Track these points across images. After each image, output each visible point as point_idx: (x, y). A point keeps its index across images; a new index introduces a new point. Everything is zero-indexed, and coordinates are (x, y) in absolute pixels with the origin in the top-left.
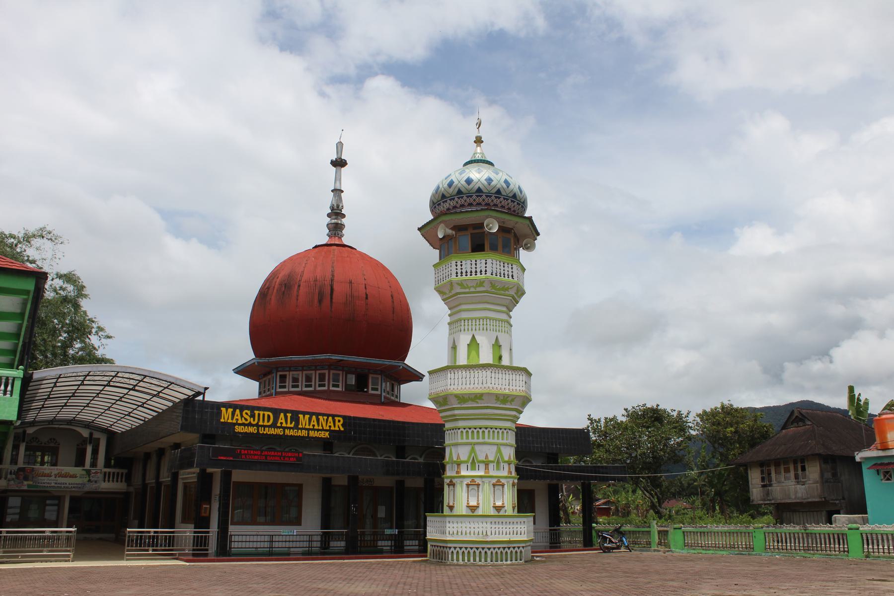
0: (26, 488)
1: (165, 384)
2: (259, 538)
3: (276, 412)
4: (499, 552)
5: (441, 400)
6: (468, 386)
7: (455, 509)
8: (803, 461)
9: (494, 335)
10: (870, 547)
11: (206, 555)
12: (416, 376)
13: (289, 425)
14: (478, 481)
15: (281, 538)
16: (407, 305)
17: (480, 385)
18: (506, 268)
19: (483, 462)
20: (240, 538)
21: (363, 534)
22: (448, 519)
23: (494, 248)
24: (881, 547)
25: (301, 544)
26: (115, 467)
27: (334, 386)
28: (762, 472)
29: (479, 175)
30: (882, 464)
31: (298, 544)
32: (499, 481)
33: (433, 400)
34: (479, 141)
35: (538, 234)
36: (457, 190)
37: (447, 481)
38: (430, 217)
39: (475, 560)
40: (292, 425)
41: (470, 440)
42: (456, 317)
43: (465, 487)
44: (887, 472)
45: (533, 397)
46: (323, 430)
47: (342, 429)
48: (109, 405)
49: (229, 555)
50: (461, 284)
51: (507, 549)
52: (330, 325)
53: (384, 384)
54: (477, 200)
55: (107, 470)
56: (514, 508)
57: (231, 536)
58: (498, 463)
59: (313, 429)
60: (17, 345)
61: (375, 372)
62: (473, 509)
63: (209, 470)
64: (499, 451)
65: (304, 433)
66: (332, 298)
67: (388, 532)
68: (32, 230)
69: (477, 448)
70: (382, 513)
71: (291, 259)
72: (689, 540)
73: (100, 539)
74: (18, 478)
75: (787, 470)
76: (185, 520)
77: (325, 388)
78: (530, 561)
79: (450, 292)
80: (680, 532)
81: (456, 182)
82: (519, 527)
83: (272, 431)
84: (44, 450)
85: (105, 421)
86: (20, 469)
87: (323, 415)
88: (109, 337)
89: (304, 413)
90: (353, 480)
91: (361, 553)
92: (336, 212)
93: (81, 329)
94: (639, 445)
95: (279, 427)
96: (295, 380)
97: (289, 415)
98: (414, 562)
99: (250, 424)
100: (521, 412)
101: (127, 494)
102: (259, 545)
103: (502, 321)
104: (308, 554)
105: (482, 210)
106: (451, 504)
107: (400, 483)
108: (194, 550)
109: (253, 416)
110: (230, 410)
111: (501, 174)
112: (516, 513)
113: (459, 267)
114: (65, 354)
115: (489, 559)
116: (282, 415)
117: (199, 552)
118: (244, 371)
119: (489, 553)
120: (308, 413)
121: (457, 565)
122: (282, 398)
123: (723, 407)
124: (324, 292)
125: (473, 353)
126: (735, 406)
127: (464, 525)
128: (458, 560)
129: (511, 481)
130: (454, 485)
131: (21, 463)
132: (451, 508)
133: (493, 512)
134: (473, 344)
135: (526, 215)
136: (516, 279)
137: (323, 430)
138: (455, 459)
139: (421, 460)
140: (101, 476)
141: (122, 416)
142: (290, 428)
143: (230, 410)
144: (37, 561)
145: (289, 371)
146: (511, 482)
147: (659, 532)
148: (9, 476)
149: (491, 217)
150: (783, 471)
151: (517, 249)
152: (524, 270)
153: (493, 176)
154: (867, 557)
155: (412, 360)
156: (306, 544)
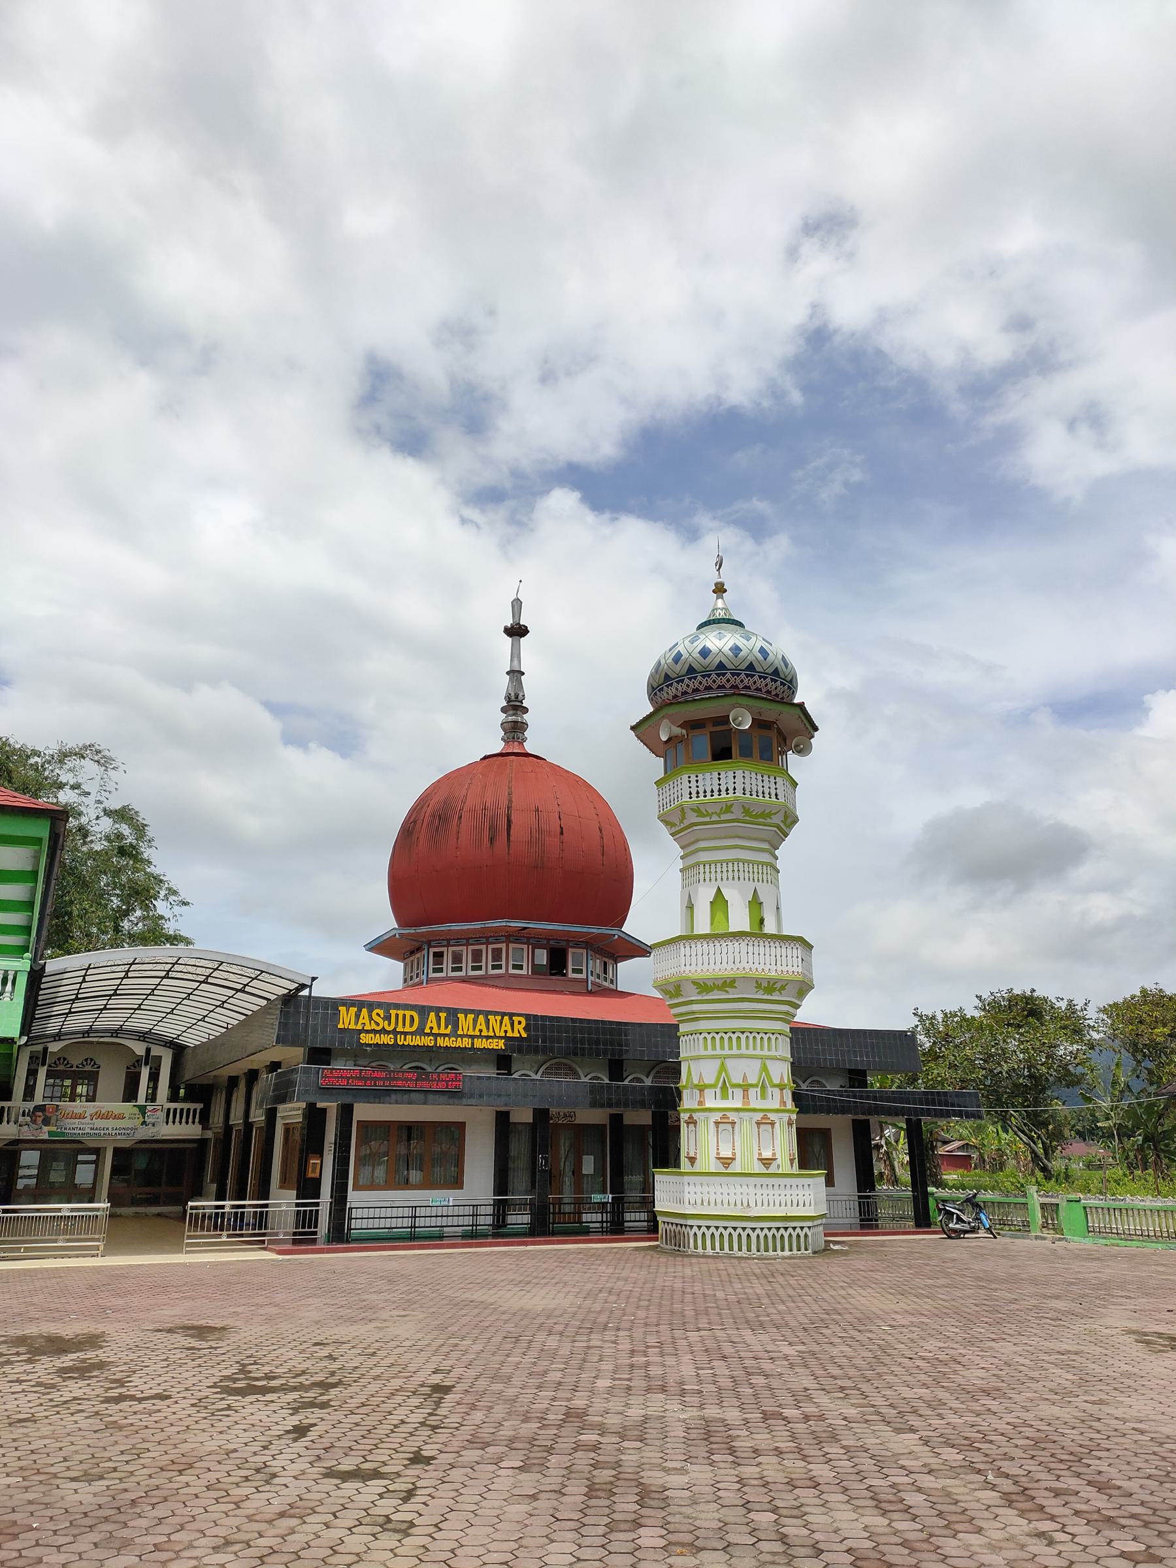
0: (46, 1137)
1: (253, 974)
2: (395, 1212)
3: (424, 1011)
4: (770, 1235)
5: (672, 988)
6: (706, 966)
7: (697, 1162)
9: (751, 886)
11: (314, 1241)
12: (638, 950)
13: (442, 1031)
14: (732, 1116)
15: (428, 1212)
16: (626, 849)
17: (731, 965)
18: (766, 784)
19: (739, 1086)
20: (365, 1213)
21: (560, 1202)
22: (686, 1179)
23: (746, 753)
25: (461, 1221)
26: (185, 1099)
27: (515, 967)
29: (720, 642)
31: (455, 1221)
33: (659, 988)
34: (720, 590)
35: (816, 729)
36: (687, 666)
37: (684, 1116)
38: (650, 709)
39: (731, 1249)
40: (448, 1031)
42: (691, 860)
43: (712, 1126)
45: (817, 975)
46: (495, 1037)
47: (524, 1035)
48: (173, 1006)
49: (348, 1242)
50: (697, 810)
51: (782, 1231)
52: (500, 871)
53: (591, 962)
54: (718, 682)
55: (173, 1105)
56: (792, 1161)
57: (351, 1209)
58: (763, 1087)
59: (480, 1036)
60: (31, 918)
61: (577, 945)
62: (727, 1162)
63: (320, 1105)
64: (764, 1068)
65: (466, 1043)
66: (509, 835)
67: (597, 1198)
68: (72, 743)
69: (729, 1063)
70: (588, 1165)
71: (448, 778)
72: (1095, 1221)
73: (159, 1215)
74: (34, 1122)
76: (284, 1184)
77: (502, 971)
78: (824, 1251)
79: (681, 822)
80: (1078, 1208)
81: (685, 655)
82: (801, 1193)
83: (418, 1041)
84: (77, 1076)
85: (169, 1029)
86: (41, 1108)
87: (496, 1013)
88: (185, 904)
89: (466, 1012)
90: (541, 1115)
91: (553, 1234)
92: (515, 704)
93: (142, 893)
94: (1004, 1055)
95: (428, 1035)
96: (457, 958)
97: (443, 1015)
98: (637, 1249)
99: (384, 1031)
100: (797, 1007)
101: (203, 1143)
102: (394, 1223)
103: (763, 864)
104: (472, 1236)
105: (726, 696)
107: (616, 1119)
108: (295, 1234)
109: (388, 1018)
110: (353, 1010)
111: (754, 639)
112: (795, 1170)
113: (693, 784)
114: (117, 929)
115: (754, 1247)
116: (432, 1015)
117: (304, 1234)
118: (381, 947)
119: (753, 1236)
120: (471, 1011)
121: (704, 1256)
122: (435, 988)
123: (1144, 992)
124: (499, 826)
125: (720, 916)
126: (1168, 992)
127: (712, 1189)
128: (704, 1248)
129: (785, 1117)
130: (695, 1123)
131: (38, 1100)
132: (692, 1160)
133: (758, 1168)
134: (719, 902)
135: (796, 701)
136: (782, 800)
137: (495, 1037)
138: (696, 1082)
139: (648, 1082)
140: (162, 1115)
141: (195, 1023)
142: (445, 1035)
143: (353, 1010)
144: (48, 1257)
145: (448, 946)
146: (786, 1119)
147: (1043, 1206)
148: (21, 1119)
149: (741, 706)
151: (784, 753)
152: (795, 784)
153: (741, 642)
155: (637, 925)
156: (468, 1220)
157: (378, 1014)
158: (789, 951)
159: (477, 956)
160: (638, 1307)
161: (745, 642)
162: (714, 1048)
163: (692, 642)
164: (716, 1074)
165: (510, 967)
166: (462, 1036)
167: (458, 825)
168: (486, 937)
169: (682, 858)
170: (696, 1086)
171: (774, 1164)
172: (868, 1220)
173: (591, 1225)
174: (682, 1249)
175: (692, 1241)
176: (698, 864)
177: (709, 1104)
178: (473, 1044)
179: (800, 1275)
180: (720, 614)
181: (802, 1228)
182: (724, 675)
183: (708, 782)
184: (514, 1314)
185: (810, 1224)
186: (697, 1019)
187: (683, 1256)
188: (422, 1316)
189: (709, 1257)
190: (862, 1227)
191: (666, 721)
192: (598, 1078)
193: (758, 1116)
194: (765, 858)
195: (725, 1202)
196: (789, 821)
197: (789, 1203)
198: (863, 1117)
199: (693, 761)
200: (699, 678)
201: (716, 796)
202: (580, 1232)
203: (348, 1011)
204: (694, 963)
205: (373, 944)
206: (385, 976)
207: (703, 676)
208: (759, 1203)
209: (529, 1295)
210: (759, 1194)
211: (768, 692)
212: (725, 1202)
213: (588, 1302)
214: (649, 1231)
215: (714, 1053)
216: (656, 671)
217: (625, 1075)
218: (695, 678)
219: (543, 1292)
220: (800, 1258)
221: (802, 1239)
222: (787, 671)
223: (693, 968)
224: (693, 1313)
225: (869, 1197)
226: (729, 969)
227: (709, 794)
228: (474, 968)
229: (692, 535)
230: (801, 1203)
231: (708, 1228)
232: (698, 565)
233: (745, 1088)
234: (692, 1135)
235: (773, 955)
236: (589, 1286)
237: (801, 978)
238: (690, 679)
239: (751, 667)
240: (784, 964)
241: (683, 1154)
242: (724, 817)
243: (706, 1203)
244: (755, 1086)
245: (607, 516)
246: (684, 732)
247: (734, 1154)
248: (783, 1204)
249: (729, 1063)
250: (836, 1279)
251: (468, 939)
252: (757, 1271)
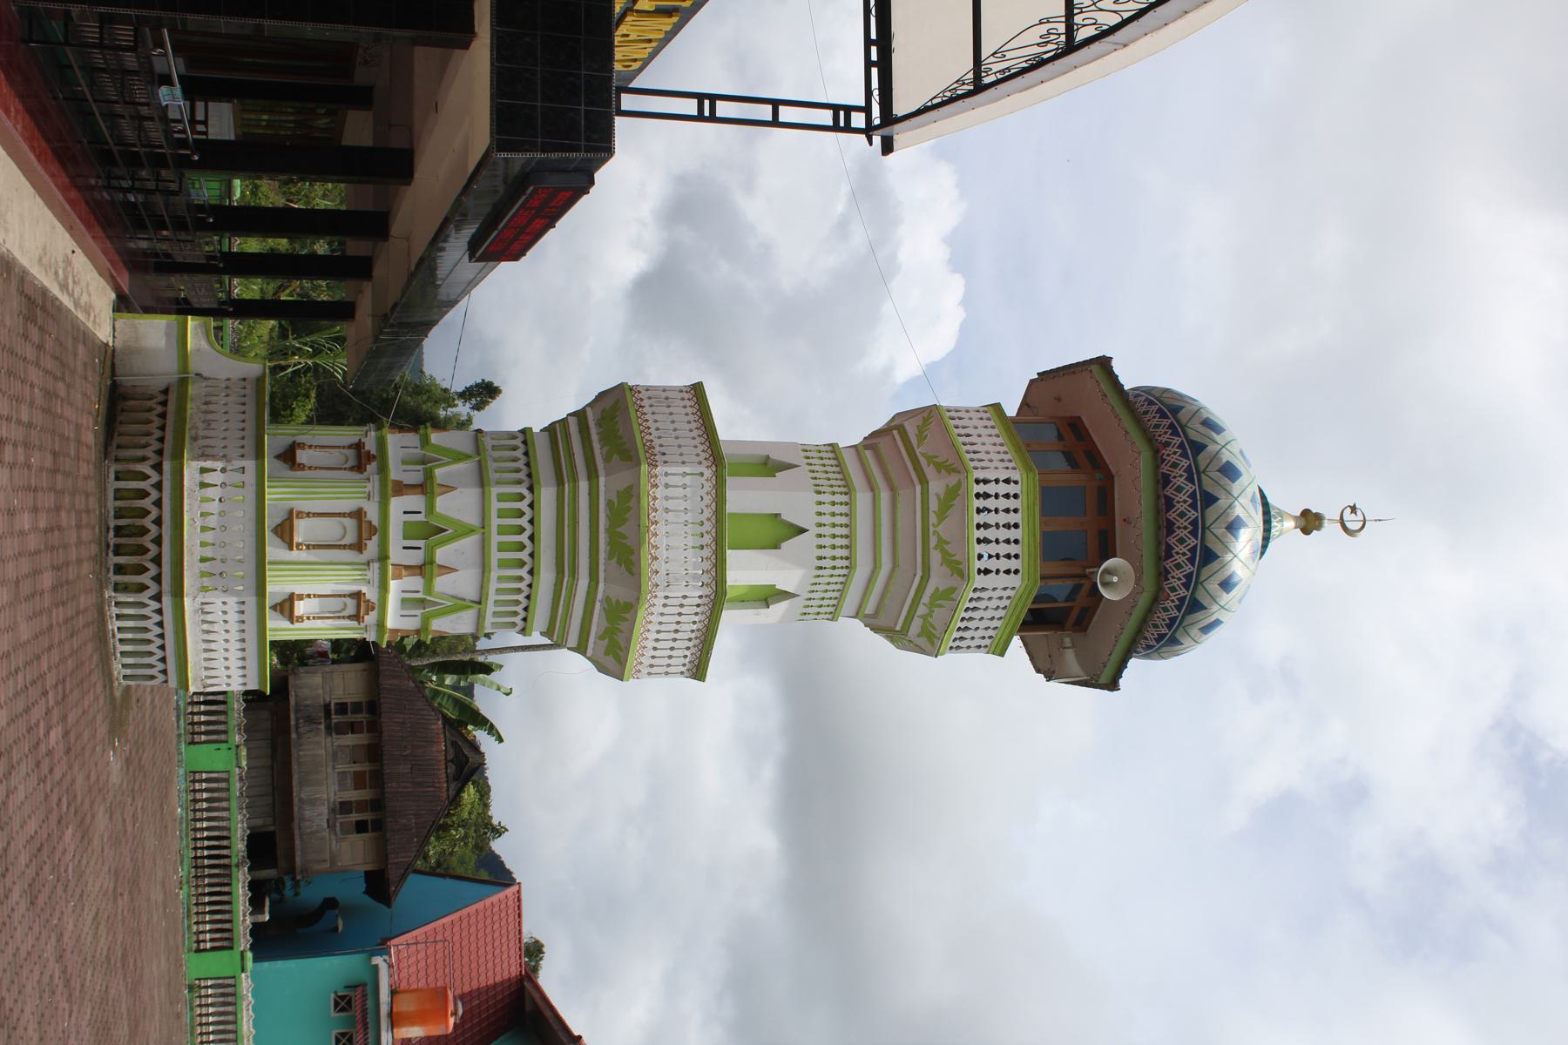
8: (378, 826)
10: (205, 805)
14: (372, 546)
19: (429, 475)
24: (211, 1010)
28: (357, 707)
30: (365, 996)
32: (373, 530)
34: (1310, 522)
39: (123, 654)
41: (495, 522)
43: (355, 588)
44: (349, 1003)
58: (422, 603)
62: (285, 530)
75: (359, 781)
81: (1225, 598)
106: (302, 456)
130: (359, 467)
150: (357, 768)
154: (191, 988)
176: (849, 490)
177: (394, 585)
181: (160, 624)
207: (1194, 523)
215: (494, 514)
218: (1191, 560)
222: (1194, 631)
244: (429, 588)
247: (300, 619)
249: (469, 544)
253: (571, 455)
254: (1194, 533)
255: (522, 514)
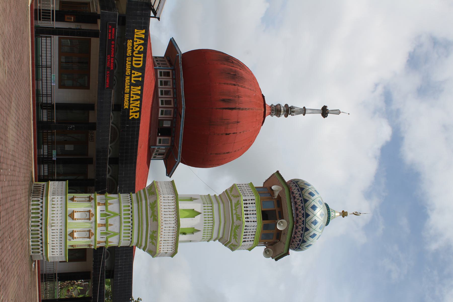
2: (49, 58)
3: (142, 70)
4: (39, 236)
6: (163, 210)
7: (71, 202)
9: (201, 228)
11: (36, 19)
13: (133, 79)
14: (93, 219)
18: (250, 236)
19: (107, 222)
20: (49, 44)
21: (53, 134)
23: (265, 227)
25: (44, 89)
29: (319, 214)
31: (44, 86)
33: (153, 184)
34: (344, 214)
35: (276, 260)
36: (307, 199)
37: (93, 196)
39: (32, 218)
40: (133, 81)
41: (123, 212)
42: (214, 200)
43: (88, 209)
46: (130, 104)
47: (130, 118)
49: (36, 36)
50: (238, 203)
51: (41, 241)
52: (207, 105)
53: (164, 148)
56: (72, 246)
57: (51, 37)
58: (106, 234)
61: (172, 141)
62: (72, 216)
63: (99, 21)
64: (115, 234)
65: (127, 90)
66: (226, 109)
67: (54, 152)
69: (117, 218)
70: (68, 147)
71: (254, 78)
77: (160, 105)
79: (232, 195)
81: (313, 198)
82: (58, 250)
83: (128, 67)
87: (141, 104)
89: (141, 90)
90: (93, 127)
91: (38, 133)
92: (289, 111)
95: (131, 72)
96: (166, 83)
97: (140, 79)
98: (32, 172)
99: (133, 51)
100: (144, 250)
102: (44, 57)
104: (37, 94)
105: (293, 218)
106: (75, 199)
107: (90, 161)
108: (40, 10)
109: (139, 53)
111: (320, 231)
112: (68, 247)
113: (251, 202)
115: (33, 228)
116: (140, 74)
118: (172, 45)
119: (38, 228)
121: (29, 205)
124: (230, 103)
125: (187, 214)
127: (59, 209)
128: (33, 205)
132: (72, 199)
133: (69, 230)
134: (194, 213)
136: (243, 244)
137: (130, 104)
138: (109, 201)
139: (108, 176)
142: (131, 80)
143: (143, 36)
145: (173, 79)
146: (92, 244)
149: (288, 225)
151: (265, 244)
152: (250, 249)
153: (318, 225)
155: (182, 168)
157: (141, 48)
158: (171, 247)
159: (167, 93)
160: (9, 181)
161: (319, 227)
162: (125, 210)
163: (319, 201)
164: (112, 211)
165: (162, 109)
166: (130, 88)
167: (231, 84)
168: (177, 97)
169: (215, 195)
170: (107, 201)
171: (71, 238)
172: (45, 277)
173: (42, 150)
174: (32, 194)
175: (36, 199)
177: (98, 208)
178: (127, 93)
179: (22, 252)
180: (332, 214)
181: (42, 243)
182: (303, 217)
183: (252, 209)
184: (6, 124)
185: (44, 254)
186: (138, 202)
187: (29, 195)
188: (5, 81)
189: (29, 207)
190: (42, 275)
191: (281, 189)
192: (110, 153)
193: (93, 231)
194: (215, 236)
195: (54, 215)
196: (232, 247)
197: (53, 245)
198: (92, 277)
199: (262, 202)
200: (302, 205)
201: (245, 212)
202: (39, 144)
203: (143, 34)
204: (165, 201)
205: (173, 42)
206: (159, 49)
207: (302, 207)
208: (53, 231)
209: (13, 128)
210: (57, 231)
211: (294, 238)
212: (54, 215)
213: (10, 157)
214: (39, 176)
215: (122, 211)
216: (306, 184)
217: (111, 165)
218: (302, 203)
219: (15, 134)
220: (29, 250)
221: (37, 251)
222: (304, 247)
223: (162, 201)
224: (7, 207)
225: (55, 278)
226: (162, 218)
227: (246, 209)
228: (162, 91)
229: (368, 195)
230: (53, 250)
231: (42, 207)
232: (355, 201)
233: (105, 225)
234: (83, 199)
235: (169, 239)
236: (17, 155)
237: (158, 251)
238: (301, 200)
239: (307, 230)
240: (164, 244)
241: (75, 195)
242: (235, 217)
243: (53, 206)
245: (378, 153)
246: (276, 197)
247: (75, 219)
248: (53, 242)
250: (21, 269)
251: (176, 88)
252: (23, 232)
253: (142, 235)
254: (303, 209)
255: (129, 206)
